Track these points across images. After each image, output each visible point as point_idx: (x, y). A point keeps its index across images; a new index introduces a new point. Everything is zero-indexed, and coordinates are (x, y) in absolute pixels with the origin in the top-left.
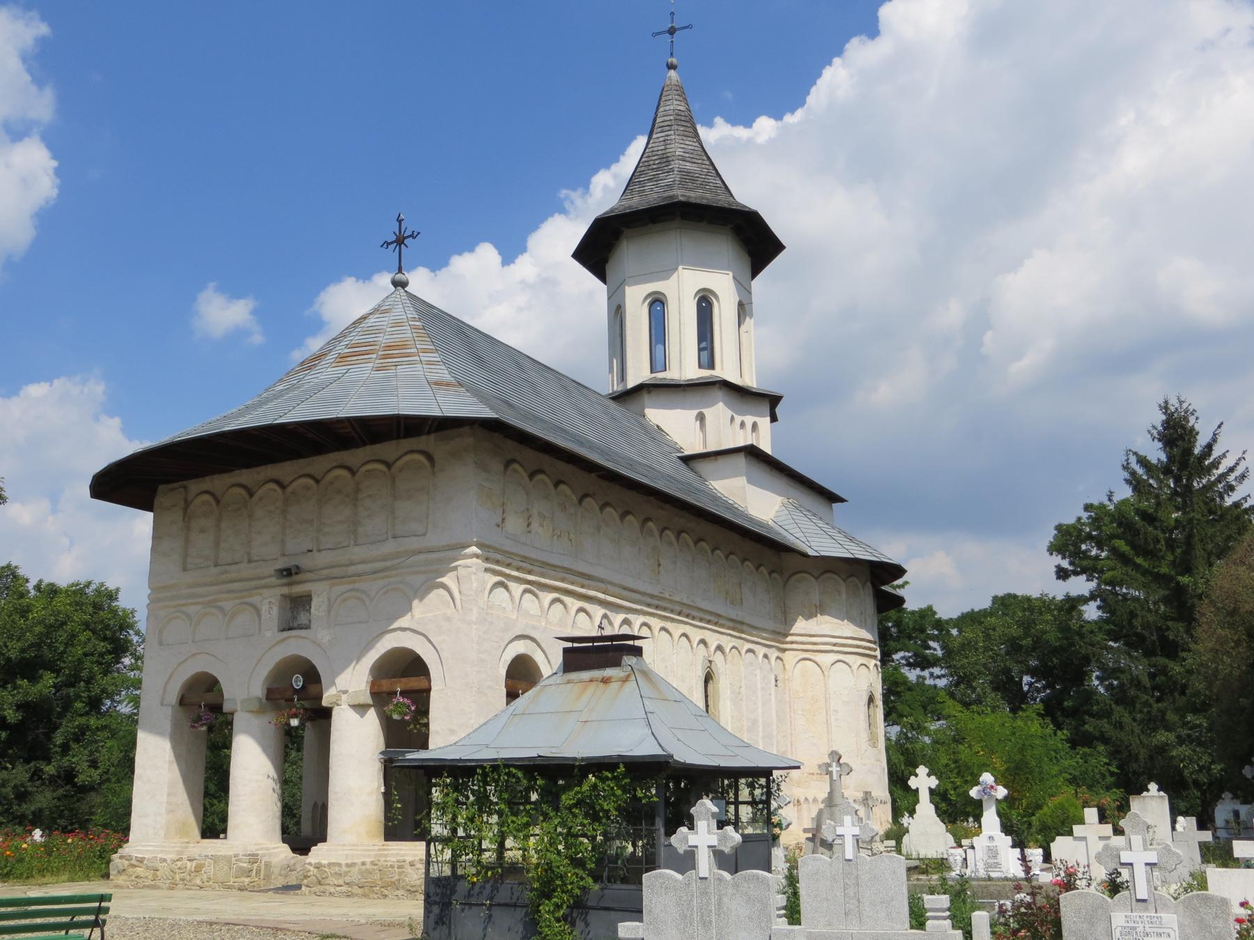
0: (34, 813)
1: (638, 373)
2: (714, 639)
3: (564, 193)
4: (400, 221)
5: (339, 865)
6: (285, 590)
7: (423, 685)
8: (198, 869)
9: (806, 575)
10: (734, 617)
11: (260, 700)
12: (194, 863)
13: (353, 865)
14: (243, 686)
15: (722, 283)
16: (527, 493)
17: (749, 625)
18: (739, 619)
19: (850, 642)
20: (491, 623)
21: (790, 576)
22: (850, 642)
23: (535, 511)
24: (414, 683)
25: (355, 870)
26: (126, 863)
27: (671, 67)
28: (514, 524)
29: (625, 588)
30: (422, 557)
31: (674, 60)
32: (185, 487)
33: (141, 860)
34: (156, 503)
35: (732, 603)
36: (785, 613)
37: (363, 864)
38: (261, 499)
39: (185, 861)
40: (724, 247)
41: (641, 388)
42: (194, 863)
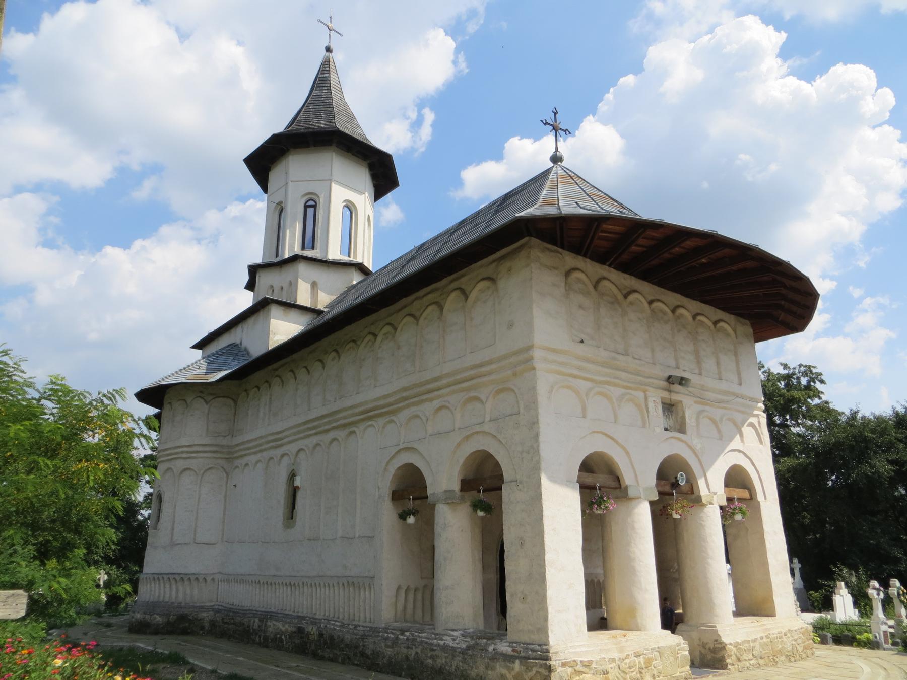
1: (292, 246)
5: (748, 642)
6: (665, 395)
8: (648, 662)
12: (642, 659)
13: (755, 641)
14: (443, 478)
15: (363, 201)
19: (201, 449)
22: (243, 453)
24: (589, 479)
25: (757, 644)
26: (570, 670)
33: (587, 665)
37: (762, 638)
38: (631, 303)
39: (633, 658)
40: (362, 177)
41: (295, 259)
42: (642, 659)
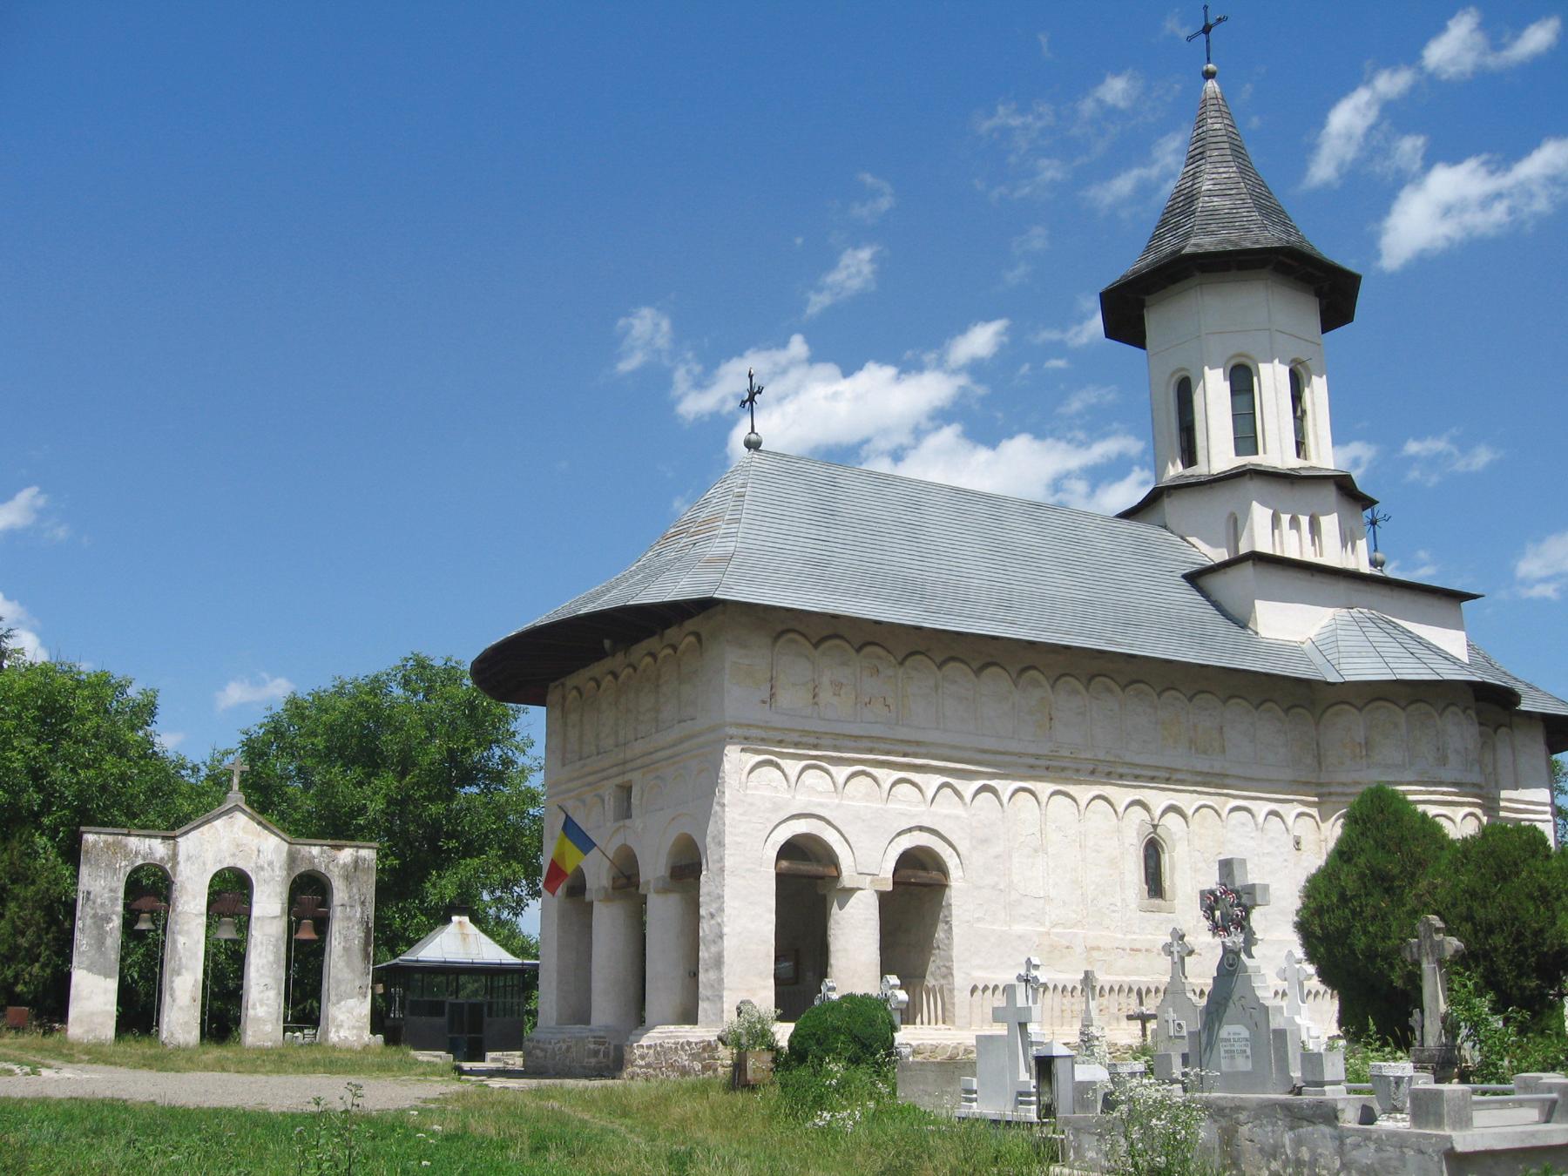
0: (1216, 928)
2: (1158, 799)
3: (622, 322)
4: (751, 376)
7: (784, 864)
9: (1346, 707)
10: (1206, 770)
11: (606, 889)
16: (807, 657)
17: (1239, 777)
18: (1217, 770)
20: (751, 804)
21: (1324, 711)
23: (825, 680)
27: (1209, 75)
28: (791, 698)
29: (985, 751)
30: (686, 745)
31: (1211, 66)
32: (563, 685)
34: (549, 698)
35: (1205, 752)
36: (1319, 759)
